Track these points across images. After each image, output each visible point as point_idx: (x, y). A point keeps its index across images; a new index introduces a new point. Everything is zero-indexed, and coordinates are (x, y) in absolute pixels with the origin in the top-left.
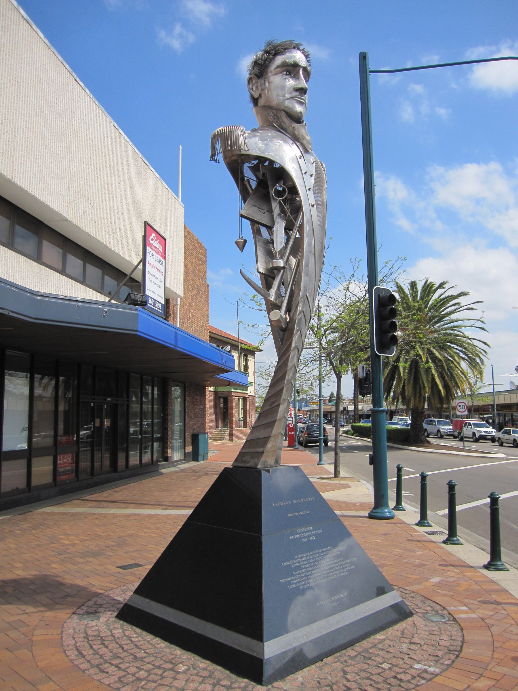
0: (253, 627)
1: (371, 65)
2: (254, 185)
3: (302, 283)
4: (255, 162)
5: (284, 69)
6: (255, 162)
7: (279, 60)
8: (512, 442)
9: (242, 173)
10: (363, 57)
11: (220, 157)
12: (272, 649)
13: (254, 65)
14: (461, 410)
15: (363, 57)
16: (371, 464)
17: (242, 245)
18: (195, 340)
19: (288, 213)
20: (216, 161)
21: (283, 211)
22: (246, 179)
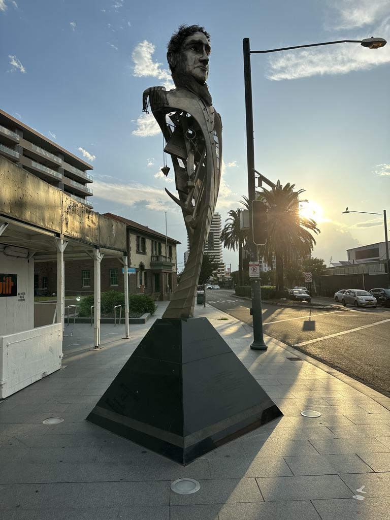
0: (179, 429)
1: (252, 48)
2: (173, 129)
3: (163, 283)
4: (174, 113)
5: (193, 45)
6: (174, 113)
7: (190, 39)
8: (353, 302)
9: (165, 120)
10: (246, 42)
11: (149, 109)
12: (190, 441)
13: (172, 43)
14: (308, 279)
15: (246, 42)
16: (251, 315)
17: (166, 171)
18: (47, 233)
19: (196, 150)
20: (147, 111)
21: (192, 147)
22: (168, 125)
